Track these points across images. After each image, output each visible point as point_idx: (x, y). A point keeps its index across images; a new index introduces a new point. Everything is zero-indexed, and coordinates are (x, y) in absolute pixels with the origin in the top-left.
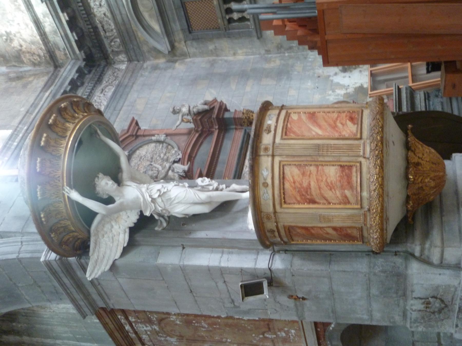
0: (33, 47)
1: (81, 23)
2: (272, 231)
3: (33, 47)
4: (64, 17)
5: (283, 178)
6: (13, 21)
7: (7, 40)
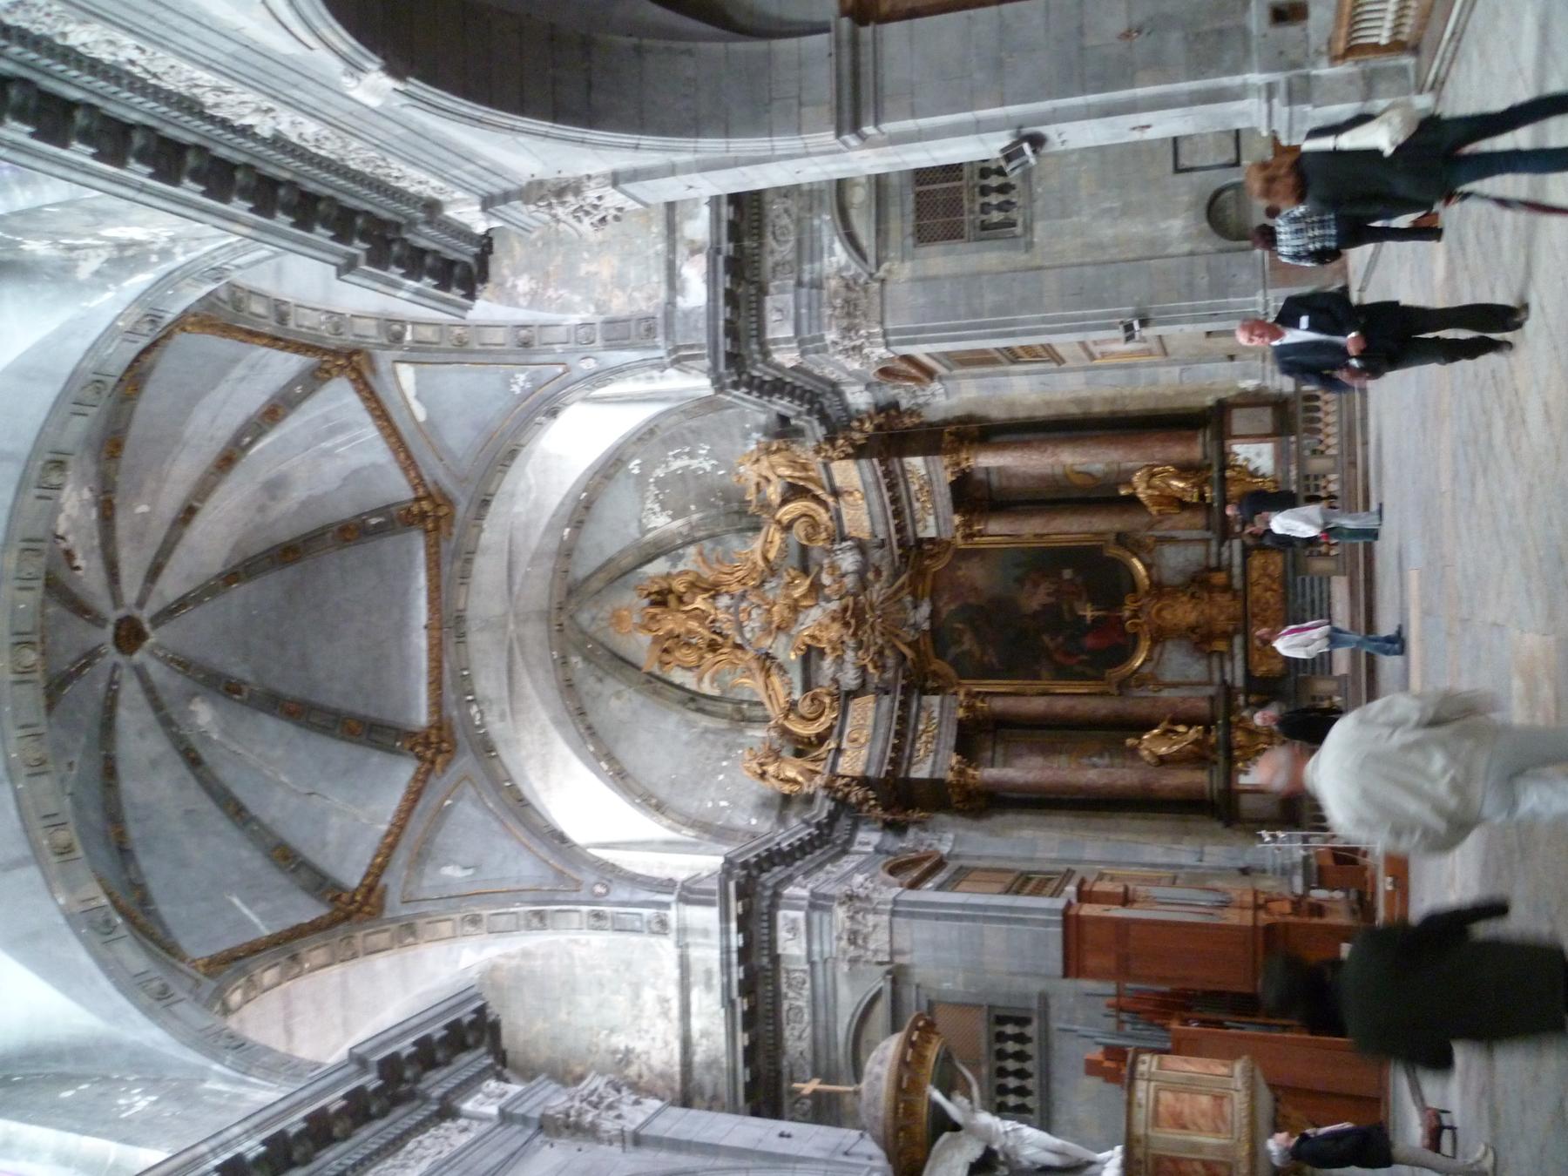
0: (660, 1083)
1: (761, 1060)
2: (1140, 1162)
3: (660, 1083)
4: (743, 1039)
5: (1157, 1101)
6: (647, 1032)
7: (621, 1060)
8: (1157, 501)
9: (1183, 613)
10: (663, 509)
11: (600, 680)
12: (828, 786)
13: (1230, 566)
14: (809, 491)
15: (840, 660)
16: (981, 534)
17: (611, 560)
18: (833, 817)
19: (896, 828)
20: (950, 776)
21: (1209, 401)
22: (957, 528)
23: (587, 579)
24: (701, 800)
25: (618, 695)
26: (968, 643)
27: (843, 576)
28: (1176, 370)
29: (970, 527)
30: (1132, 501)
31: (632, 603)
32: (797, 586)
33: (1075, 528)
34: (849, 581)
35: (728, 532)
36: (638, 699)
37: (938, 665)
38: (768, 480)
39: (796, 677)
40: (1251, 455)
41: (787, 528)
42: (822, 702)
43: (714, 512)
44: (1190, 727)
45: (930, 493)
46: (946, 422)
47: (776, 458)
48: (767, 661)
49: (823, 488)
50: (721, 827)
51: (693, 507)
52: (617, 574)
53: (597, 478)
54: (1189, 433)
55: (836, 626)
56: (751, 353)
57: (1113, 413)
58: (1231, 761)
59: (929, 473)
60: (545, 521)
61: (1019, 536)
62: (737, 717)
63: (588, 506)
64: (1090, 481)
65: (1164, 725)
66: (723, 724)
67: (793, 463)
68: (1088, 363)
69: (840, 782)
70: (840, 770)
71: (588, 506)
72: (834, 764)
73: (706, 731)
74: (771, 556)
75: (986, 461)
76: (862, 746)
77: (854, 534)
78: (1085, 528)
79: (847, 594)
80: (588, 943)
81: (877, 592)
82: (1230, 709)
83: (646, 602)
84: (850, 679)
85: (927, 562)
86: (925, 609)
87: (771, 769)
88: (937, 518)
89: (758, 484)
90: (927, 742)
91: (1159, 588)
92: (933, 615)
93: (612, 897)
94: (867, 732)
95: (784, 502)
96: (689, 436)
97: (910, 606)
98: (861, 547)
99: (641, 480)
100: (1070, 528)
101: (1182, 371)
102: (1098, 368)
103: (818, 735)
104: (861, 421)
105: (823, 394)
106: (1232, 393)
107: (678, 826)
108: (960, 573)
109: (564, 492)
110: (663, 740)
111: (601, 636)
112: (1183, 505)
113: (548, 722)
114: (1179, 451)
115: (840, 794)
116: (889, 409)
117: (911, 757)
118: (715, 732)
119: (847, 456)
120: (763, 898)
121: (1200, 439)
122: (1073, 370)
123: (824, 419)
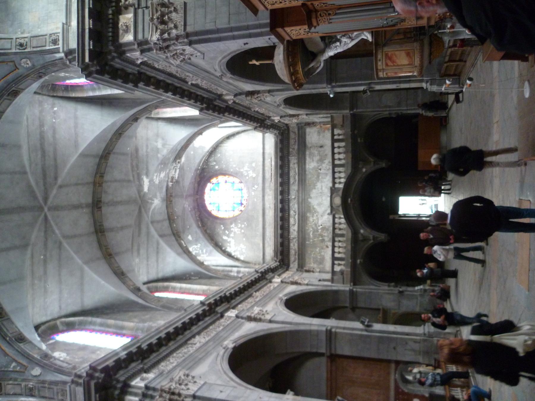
120: (115, 388)
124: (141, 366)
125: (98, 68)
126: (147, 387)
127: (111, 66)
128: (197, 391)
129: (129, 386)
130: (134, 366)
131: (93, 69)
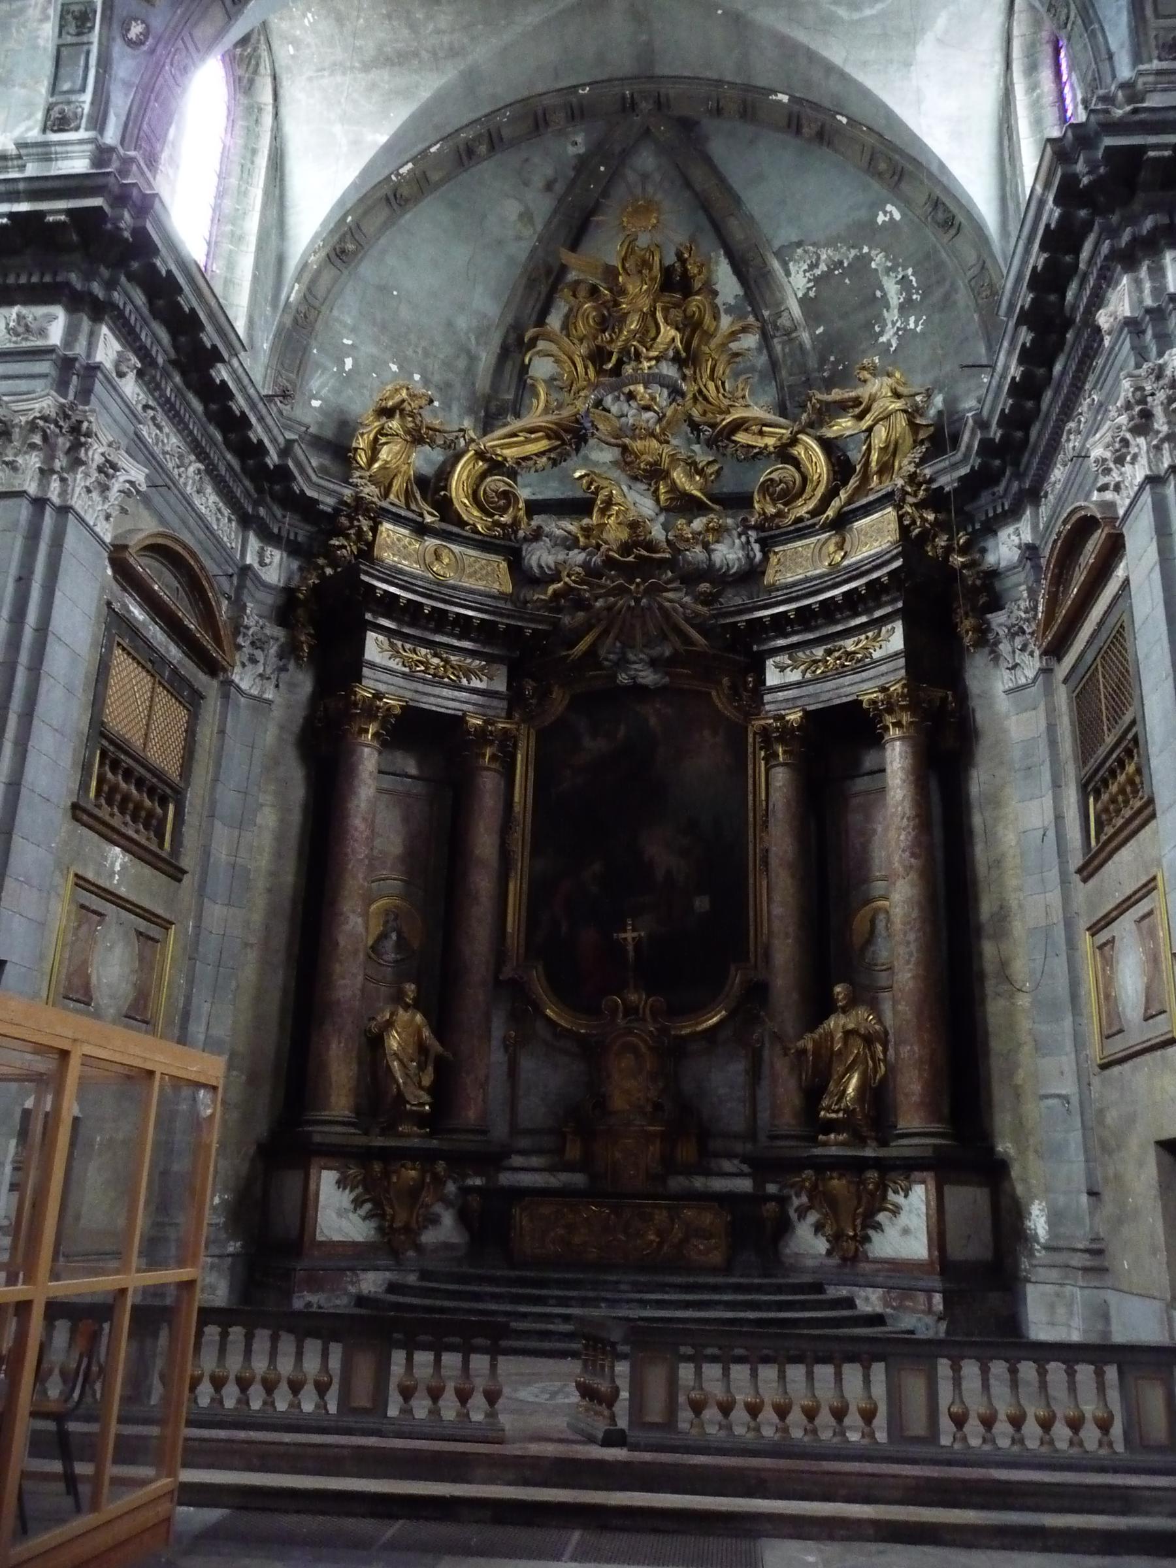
8: (823, 1046)
9: (628, 1087)
10: (817, 280)
11: (549, 187)
12: (359, 505)
13: (708, 1173)
14: (845, 483)
15: (570, 543)
16: (771, 756)
17: (737, 200)
18: (305, 508)
19: (287, 609)
20: (364, 692)
21: (1005, 1147)
22: (781, 718)
23: (708, 160)
24: (354, 330)
25: (526, 216)
26: (593, 746)
27: (706, 546)
28: (1068, 1087)
29: (781, 740)
30: (819, 1006)
31: (668, 232)
32: (690, 477)
33: (777, 910)
34: (697, 554)
35: (780, 388)
36: (521, 250)
37: (559, 699)
38: (860, 417)
39: (552, 491)
40: (904, 1219)
41: (784, 453)
42: (503, 510)
43: (812, 363)
44: (430, 1091)
45: (841, 672)
46: (962, 695)
47: (901, 421)
48: (570, 437)
49: (850, 501)
50: (306, 349)
51: (820, 330)
52: (715, 210)
53: (871, 140)
54: (946, 1111)
55: (624, 535)
56: (1134, 220)
57: (981, 977)
58: (364, 1156)
59: (876, 663)
60: (801, 36)
61: (766, 824)
62: (493, 409)
63: (825, 136)
64: (857, 940)
65: (436, 1047)
66: (483, 383)
67: (892, 450)
68: (1083, 923)
69: (365, 524)
70: (386, 527)
71: (825, 136)
72: (397, 519)
73: (473, 359)
74: (741, 437)
75: (897, 757)
76: (429, 567)
77: (774, 560)
78: (777, 925)
79: (677, 551)
80: (46, 18)
81: (678, 599)
82: (459, 1161)
83: (671, 259)
84: (540, 556)
85: (725, 681)
86: (648, 677)
87: (395, 424)
88: (798, 685)
89: (857, 402)
90: (426, 664)
91: (673, 1052)
92: (638, 691)
93: (118, 48)
94: (452, 578)
95: (827, 445)
96: (938, 294)
97: (655, 652)
98: (751, 574)
99: (866, 231)
100: (777, 902)
101: (1065, 1098)
102: (1071, 944)
103: (448, 501)
104: (963, 551)
105: (1019, 476)
106: (1020, 1189)
107: (307, 277)
108: (706, 733)
109: (849, 69)
110: (452, 281)
111: (620, 191)
112: (813, 1093)
113: (470, 59)
114: (911, 1086)
115: (344, 520)
116: (989, 591)
117: (406, 637)
118: (470, 370)
119: (904, 530)
120: (88, 276)
121: (936, 1127)
122: (1066, 899)
123: (974, 484)
124: (160, 360)
125: (1085, 180)
126: (94, 369)
127: (1087, 227)
128: (82, 521)
129: (97, 318)
130: (158, 336)
131: (1080, 167)
